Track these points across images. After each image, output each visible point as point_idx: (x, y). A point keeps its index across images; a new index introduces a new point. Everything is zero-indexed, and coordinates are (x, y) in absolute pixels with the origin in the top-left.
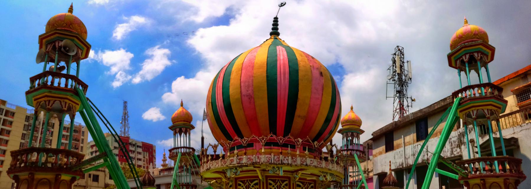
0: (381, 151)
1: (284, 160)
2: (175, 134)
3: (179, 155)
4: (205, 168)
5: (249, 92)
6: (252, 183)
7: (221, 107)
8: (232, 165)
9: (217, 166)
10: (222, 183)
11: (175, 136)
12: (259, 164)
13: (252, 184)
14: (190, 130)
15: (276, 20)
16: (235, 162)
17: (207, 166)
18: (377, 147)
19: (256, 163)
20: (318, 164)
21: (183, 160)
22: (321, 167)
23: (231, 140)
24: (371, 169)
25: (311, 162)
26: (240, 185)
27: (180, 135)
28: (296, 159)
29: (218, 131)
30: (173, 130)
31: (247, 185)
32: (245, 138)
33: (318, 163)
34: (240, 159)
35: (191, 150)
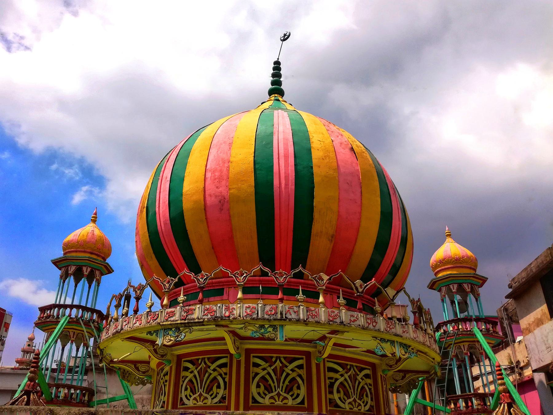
0: (539, 317)
1: (288, 314)
2: (64, 277)
3: (63, 321)
4: (112, 330)
5: (220, 189)
6: (212, 363)
7: (165, 224)
8: (169, 323)
9: (138, 324)
10: (150, 373)
11: (64, 282)
12: (229, 319)
13: (213, 366)
14: (102, 274)
15: (277, 66)
16: (177, 317)
17: (116, 327)
18: (528, 311)
19: (222, 318)
20: (369, 324)
21: (72, 334)
22: (377, 328)
23: (174, 274)
24: (526, 361)
25: (352, 319)
26: (186, 369)
27: (77, 282)
28: (318, 310)
29: (154, 263)
30: (60, 269)
31: (201, 368)
32: (203, 272)
33: (369, 321)
34: (187, 311)
35: (95, 316)
